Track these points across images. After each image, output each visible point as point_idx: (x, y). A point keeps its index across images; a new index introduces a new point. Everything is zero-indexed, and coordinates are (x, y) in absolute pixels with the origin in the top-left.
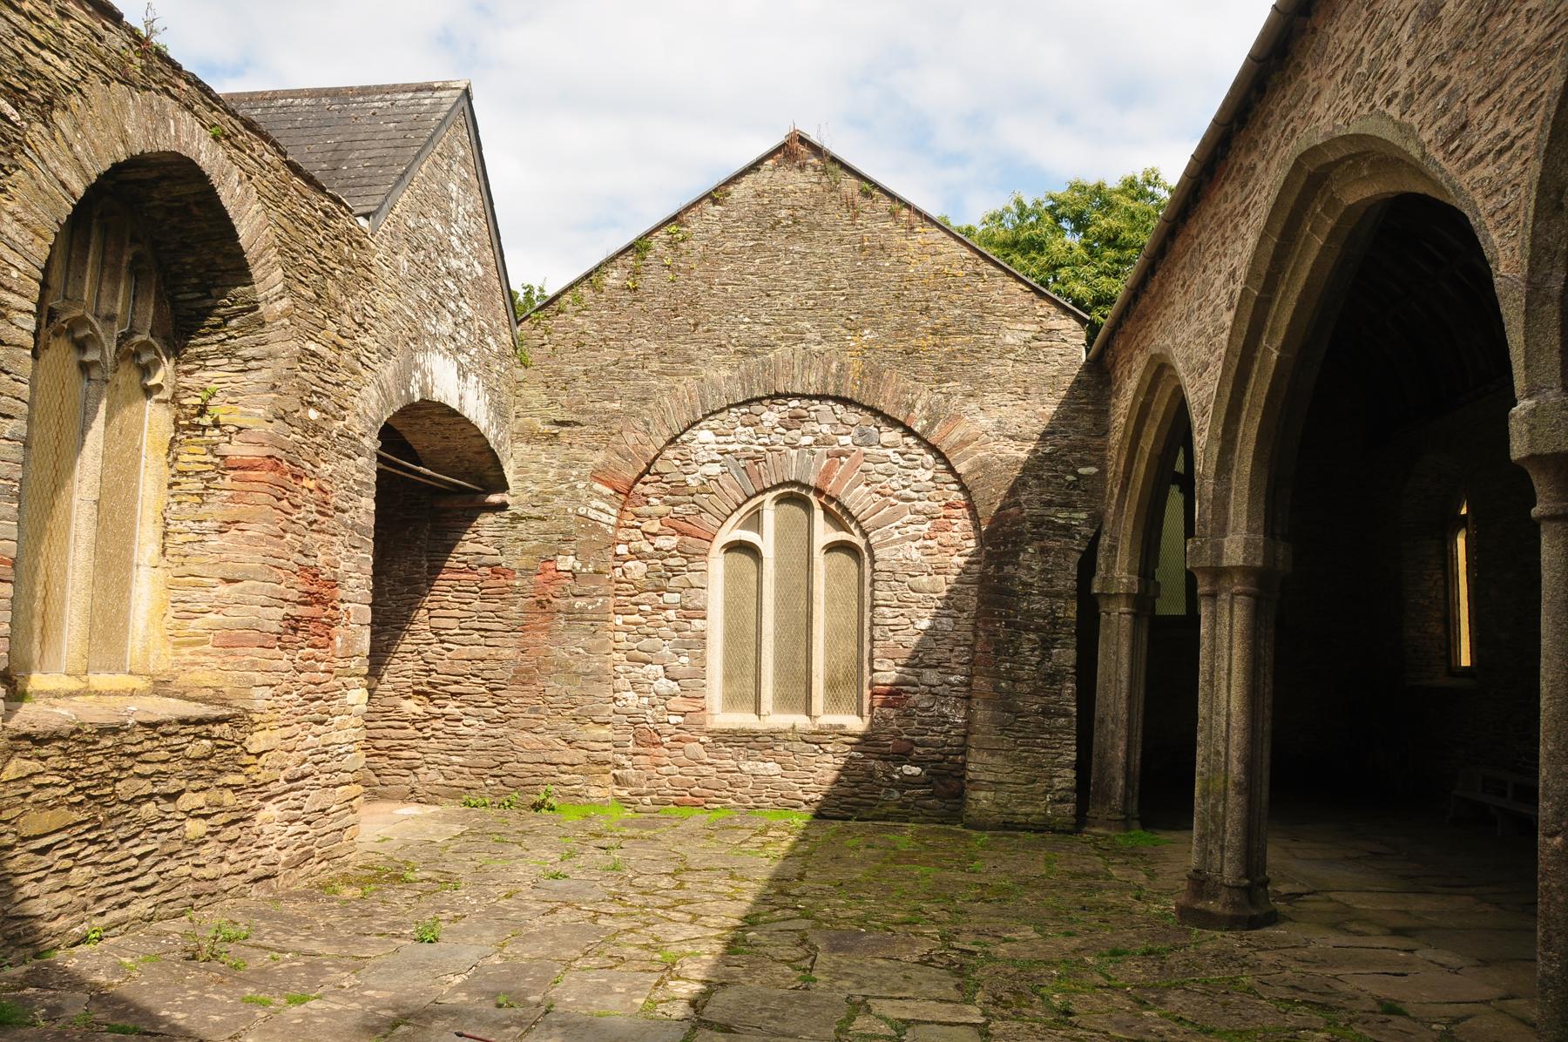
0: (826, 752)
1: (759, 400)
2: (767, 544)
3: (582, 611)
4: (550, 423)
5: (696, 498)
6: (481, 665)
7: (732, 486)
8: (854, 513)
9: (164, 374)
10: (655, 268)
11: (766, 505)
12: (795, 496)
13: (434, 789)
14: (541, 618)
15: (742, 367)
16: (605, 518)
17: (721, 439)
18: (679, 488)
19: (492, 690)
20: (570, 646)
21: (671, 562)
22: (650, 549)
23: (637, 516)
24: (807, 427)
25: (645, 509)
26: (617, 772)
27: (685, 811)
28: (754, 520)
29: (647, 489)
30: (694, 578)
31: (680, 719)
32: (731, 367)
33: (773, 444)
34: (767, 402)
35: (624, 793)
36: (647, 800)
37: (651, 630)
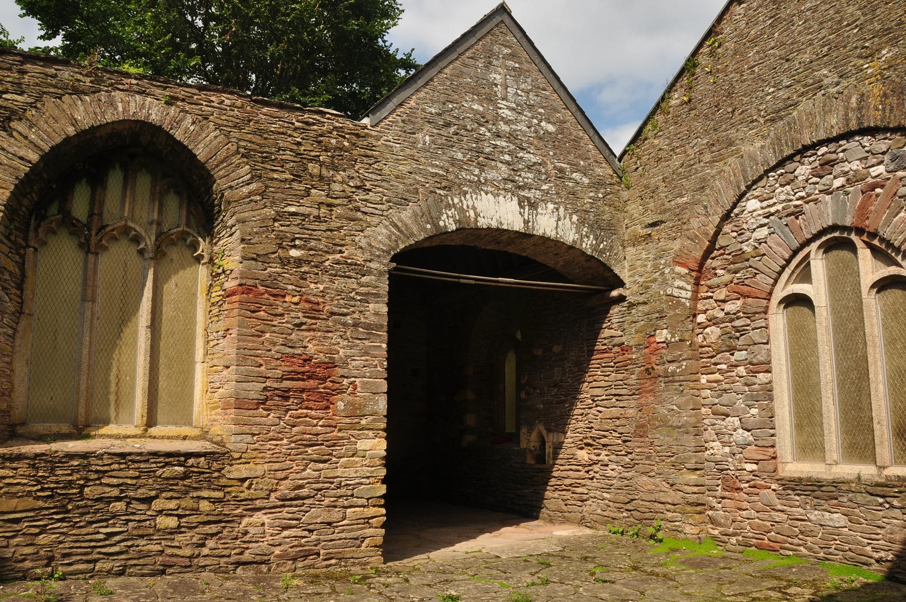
0: (892, 507)
1: (790, 158)
2: (817, 289)
3: (673, 374)
4: (646, 227)
5: (752, 262)
6: (618, 423)
7: (779, 245)
8: (896, 244)
9: (203, 246)
10: (701, 80)
11: (812, 255)
12: (837, 240)
13: (595, 517)
14: (649, 383)
15: (772, 134)
16: (684, 292)
17: (765, 204)
18: (740, 256)
19: (625, 441)
20: (670, 405)
21: (737, 323)
22: (721, 315)
23: (710, 287)
24: (837, 169)
25: (715, 281)
26: (710, 513)
27: (763, 553)
28: (805, 275)
29: (715, 263)
30: (755, 336)
31: (754, 467)
32: (763, 137)
33: (809, 195)
34: (797, 158)
35: (716, 532)
36: (733, 540)
37: (727, 386)
